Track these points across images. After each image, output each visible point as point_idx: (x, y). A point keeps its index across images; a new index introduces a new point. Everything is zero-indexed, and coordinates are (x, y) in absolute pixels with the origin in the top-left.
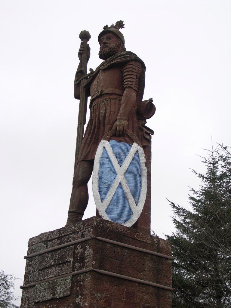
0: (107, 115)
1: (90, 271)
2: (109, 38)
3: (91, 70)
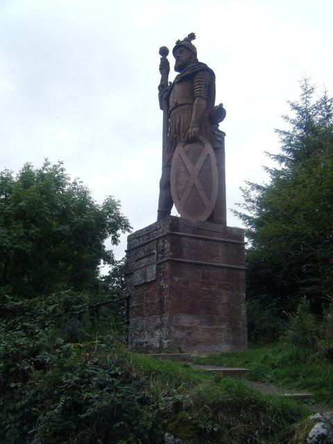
0: (181, 124)
1: (168, 261)
2: (181, 52)
3: (170, 83)
